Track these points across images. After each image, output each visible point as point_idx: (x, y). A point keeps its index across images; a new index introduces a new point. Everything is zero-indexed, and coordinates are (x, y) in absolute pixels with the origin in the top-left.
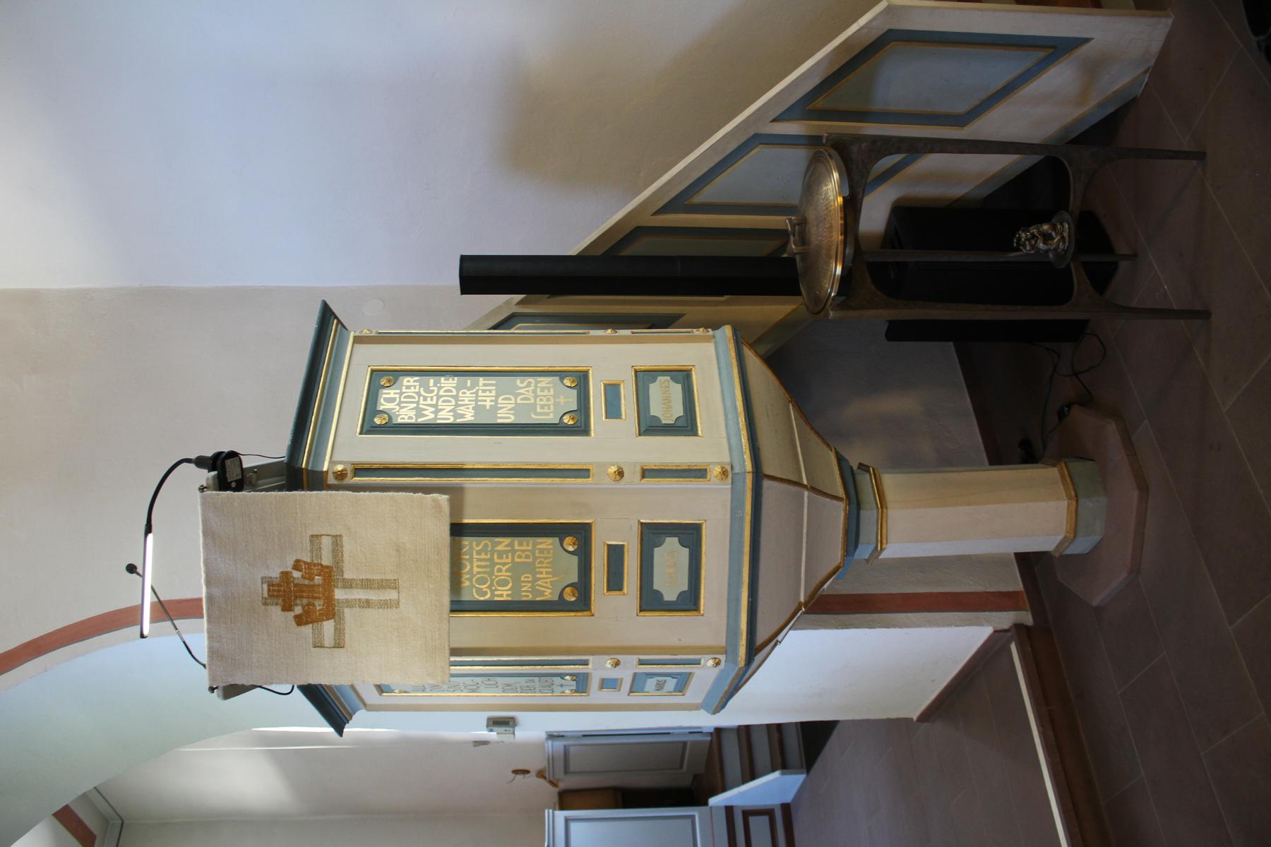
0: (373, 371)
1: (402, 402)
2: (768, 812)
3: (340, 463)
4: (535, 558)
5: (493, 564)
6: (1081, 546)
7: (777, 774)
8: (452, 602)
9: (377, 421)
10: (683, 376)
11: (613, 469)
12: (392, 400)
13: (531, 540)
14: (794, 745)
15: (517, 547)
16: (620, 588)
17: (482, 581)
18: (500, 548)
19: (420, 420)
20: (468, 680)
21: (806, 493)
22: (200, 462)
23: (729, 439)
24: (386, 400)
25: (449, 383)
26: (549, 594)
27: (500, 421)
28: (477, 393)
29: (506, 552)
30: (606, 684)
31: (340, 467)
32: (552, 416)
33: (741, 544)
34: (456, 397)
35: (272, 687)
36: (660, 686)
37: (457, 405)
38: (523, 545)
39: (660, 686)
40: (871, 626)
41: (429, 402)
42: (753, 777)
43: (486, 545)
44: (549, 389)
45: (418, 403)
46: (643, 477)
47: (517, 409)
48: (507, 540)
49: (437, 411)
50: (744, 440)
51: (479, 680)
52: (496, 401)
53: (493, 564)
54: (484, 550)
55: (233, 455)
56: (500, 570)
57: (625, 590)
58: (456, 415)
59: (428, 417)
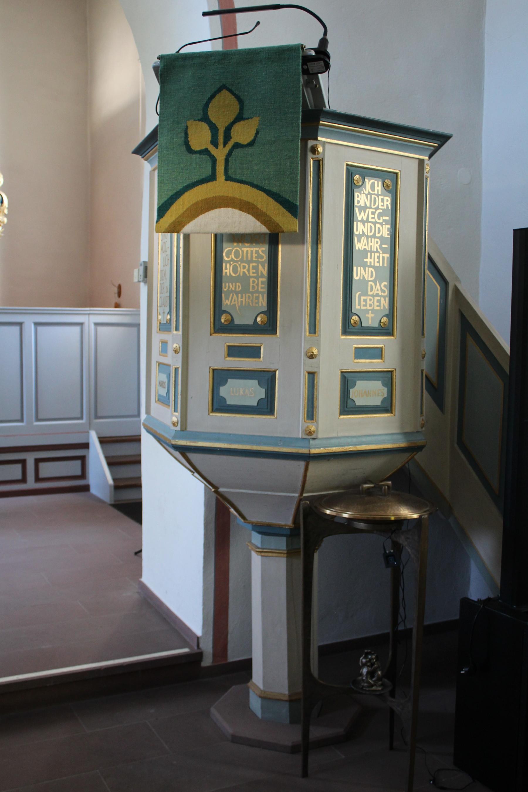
0: (396, 174)
1: (371, 197)
2: (83, 475)
4: (252, 293)
5: (249, 262)
7: (111, 481)
8: (222, 235)
9: (357, 177)
11: (315, 351)
12: (373, 187)
13: (265, 290)
14: (128, 496)
15: (260, 280)
16: (229, 355)
17: (237, 254)
18: (260, 267)
19: (356, 210)
20: (168, 244)
21: (297, 495)
22: (324, 42)
24: (373, 184)
25: (385, 231)
26: (227, 303)
27: (355, 268)
28: (377, 252)
29: (257, 272)
30: (164, 343)
31: (320, 149)
32: (358, 307)
33: (259, 444)
35: (159, 102)
36: (161, 384)
37: (368, 237)
38: (261, 284)
39: (161, 384)
41: (371, 216)
42: (110, 464)
43: (262, 257)
45: (370, 208)
46: (309, 373)
47: (364, 282)
48: (265, 272)
49: (363, 222)
51: (169, 252)
52: (370, 266)
54: (259, 256)
55: (327, 67)
56: (244, 267)
57: (228, 359)
58: (360, 237)
59: (359, 215)
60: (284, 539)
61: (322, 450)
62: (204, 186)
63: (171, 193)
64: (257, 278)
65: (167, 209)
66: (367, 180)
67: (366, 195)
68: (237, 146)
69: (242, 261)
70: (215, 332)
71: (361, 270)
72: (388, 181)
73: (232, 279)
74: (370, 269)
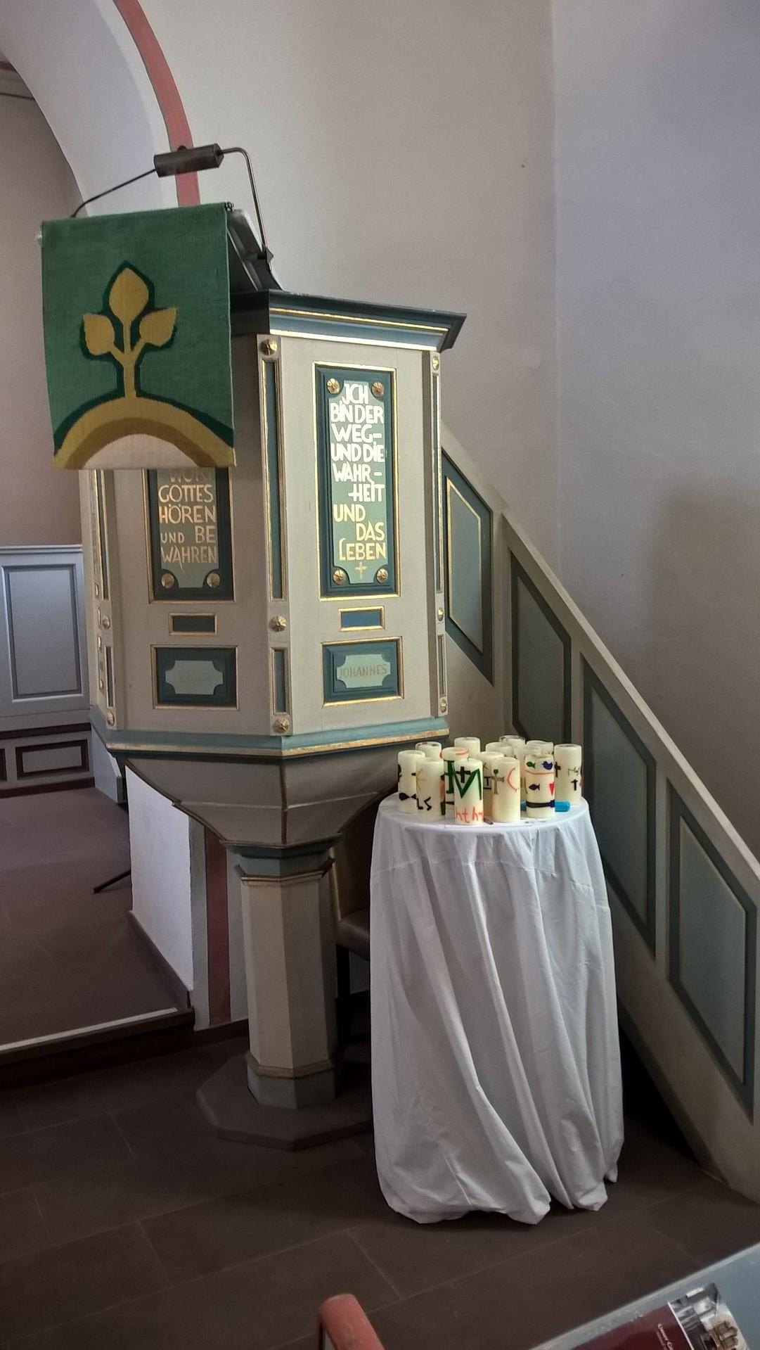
0: (391, 373)
1: (354, 409)
2: (85, 765)
3: (279, 346)
4: (199, 546)
5: (191, 504)
6: (253, 1082)
10: (393, 686)
13: (215, 542)
16: (175, 629)
17: (176, 494)
18: (207, 511)
19: (333, 427)
23: (321, 732)
24: (356, 390)
25: (378, 454)
26: (166, 559)
27: (335, 507)
31: (273, 346)
32: (342, 558)
34: (361, 461)
37: (351, 463)
38: (208, 534)
40: (193, 869)
41: (355, 434)
44: (374, 554)
45: (354, 423)
46: (276, 650)
47: (350, 524)
50: (317, 748)
52: (358, 502)
53: (191, 504)
54: (205, 496)
56: (186, 511)
59: (337, 434)
60: (277, 862)
61: (299, 751)
62: (109, 404)
63: (65, 415)
64: (204, 525)
65: (64, 436)
66: (346, 385)
67: (347, 407)
68: (149, 347)
69: (183, 503)
70: (156, 599)
71: (344, 508)
72: (378, 385)
73: (172, 528)
74: (358, 506)
